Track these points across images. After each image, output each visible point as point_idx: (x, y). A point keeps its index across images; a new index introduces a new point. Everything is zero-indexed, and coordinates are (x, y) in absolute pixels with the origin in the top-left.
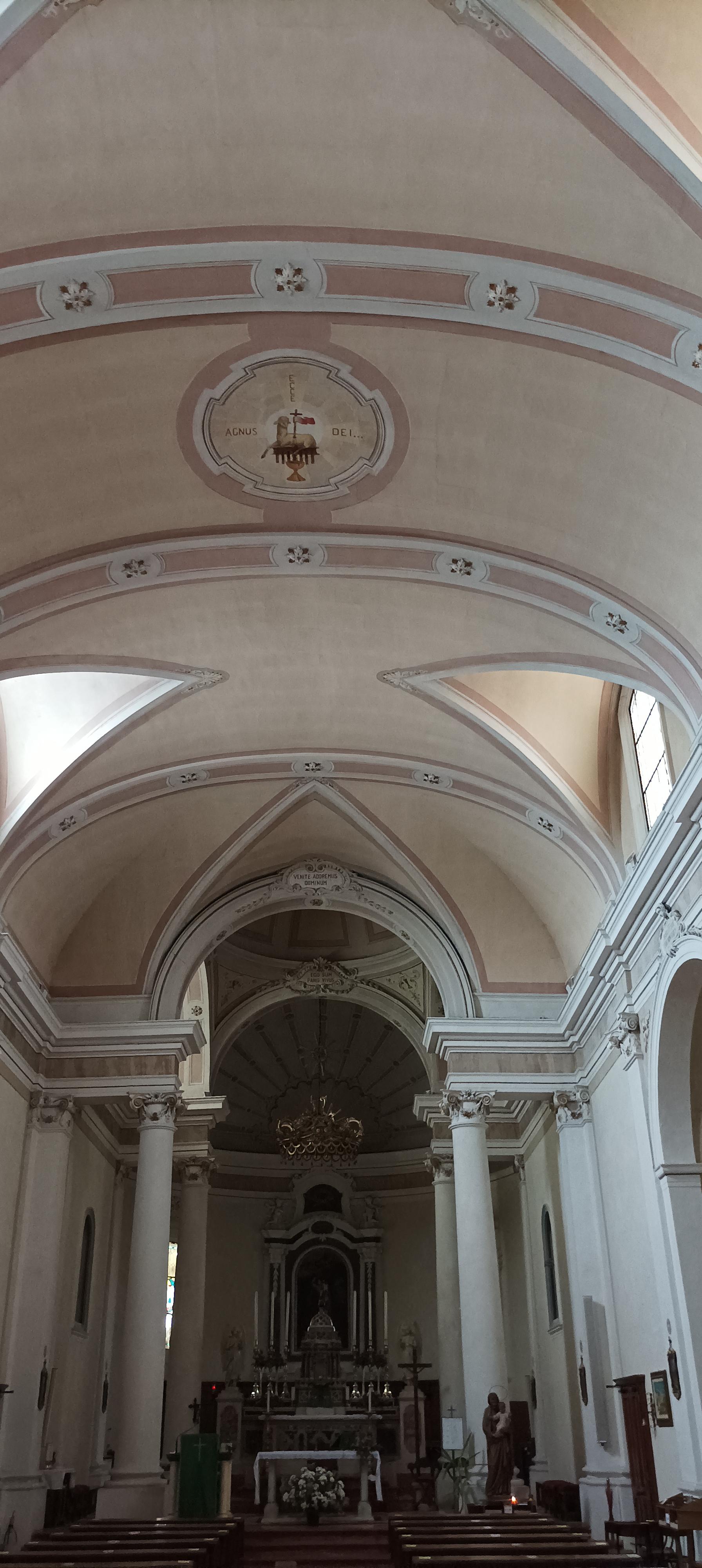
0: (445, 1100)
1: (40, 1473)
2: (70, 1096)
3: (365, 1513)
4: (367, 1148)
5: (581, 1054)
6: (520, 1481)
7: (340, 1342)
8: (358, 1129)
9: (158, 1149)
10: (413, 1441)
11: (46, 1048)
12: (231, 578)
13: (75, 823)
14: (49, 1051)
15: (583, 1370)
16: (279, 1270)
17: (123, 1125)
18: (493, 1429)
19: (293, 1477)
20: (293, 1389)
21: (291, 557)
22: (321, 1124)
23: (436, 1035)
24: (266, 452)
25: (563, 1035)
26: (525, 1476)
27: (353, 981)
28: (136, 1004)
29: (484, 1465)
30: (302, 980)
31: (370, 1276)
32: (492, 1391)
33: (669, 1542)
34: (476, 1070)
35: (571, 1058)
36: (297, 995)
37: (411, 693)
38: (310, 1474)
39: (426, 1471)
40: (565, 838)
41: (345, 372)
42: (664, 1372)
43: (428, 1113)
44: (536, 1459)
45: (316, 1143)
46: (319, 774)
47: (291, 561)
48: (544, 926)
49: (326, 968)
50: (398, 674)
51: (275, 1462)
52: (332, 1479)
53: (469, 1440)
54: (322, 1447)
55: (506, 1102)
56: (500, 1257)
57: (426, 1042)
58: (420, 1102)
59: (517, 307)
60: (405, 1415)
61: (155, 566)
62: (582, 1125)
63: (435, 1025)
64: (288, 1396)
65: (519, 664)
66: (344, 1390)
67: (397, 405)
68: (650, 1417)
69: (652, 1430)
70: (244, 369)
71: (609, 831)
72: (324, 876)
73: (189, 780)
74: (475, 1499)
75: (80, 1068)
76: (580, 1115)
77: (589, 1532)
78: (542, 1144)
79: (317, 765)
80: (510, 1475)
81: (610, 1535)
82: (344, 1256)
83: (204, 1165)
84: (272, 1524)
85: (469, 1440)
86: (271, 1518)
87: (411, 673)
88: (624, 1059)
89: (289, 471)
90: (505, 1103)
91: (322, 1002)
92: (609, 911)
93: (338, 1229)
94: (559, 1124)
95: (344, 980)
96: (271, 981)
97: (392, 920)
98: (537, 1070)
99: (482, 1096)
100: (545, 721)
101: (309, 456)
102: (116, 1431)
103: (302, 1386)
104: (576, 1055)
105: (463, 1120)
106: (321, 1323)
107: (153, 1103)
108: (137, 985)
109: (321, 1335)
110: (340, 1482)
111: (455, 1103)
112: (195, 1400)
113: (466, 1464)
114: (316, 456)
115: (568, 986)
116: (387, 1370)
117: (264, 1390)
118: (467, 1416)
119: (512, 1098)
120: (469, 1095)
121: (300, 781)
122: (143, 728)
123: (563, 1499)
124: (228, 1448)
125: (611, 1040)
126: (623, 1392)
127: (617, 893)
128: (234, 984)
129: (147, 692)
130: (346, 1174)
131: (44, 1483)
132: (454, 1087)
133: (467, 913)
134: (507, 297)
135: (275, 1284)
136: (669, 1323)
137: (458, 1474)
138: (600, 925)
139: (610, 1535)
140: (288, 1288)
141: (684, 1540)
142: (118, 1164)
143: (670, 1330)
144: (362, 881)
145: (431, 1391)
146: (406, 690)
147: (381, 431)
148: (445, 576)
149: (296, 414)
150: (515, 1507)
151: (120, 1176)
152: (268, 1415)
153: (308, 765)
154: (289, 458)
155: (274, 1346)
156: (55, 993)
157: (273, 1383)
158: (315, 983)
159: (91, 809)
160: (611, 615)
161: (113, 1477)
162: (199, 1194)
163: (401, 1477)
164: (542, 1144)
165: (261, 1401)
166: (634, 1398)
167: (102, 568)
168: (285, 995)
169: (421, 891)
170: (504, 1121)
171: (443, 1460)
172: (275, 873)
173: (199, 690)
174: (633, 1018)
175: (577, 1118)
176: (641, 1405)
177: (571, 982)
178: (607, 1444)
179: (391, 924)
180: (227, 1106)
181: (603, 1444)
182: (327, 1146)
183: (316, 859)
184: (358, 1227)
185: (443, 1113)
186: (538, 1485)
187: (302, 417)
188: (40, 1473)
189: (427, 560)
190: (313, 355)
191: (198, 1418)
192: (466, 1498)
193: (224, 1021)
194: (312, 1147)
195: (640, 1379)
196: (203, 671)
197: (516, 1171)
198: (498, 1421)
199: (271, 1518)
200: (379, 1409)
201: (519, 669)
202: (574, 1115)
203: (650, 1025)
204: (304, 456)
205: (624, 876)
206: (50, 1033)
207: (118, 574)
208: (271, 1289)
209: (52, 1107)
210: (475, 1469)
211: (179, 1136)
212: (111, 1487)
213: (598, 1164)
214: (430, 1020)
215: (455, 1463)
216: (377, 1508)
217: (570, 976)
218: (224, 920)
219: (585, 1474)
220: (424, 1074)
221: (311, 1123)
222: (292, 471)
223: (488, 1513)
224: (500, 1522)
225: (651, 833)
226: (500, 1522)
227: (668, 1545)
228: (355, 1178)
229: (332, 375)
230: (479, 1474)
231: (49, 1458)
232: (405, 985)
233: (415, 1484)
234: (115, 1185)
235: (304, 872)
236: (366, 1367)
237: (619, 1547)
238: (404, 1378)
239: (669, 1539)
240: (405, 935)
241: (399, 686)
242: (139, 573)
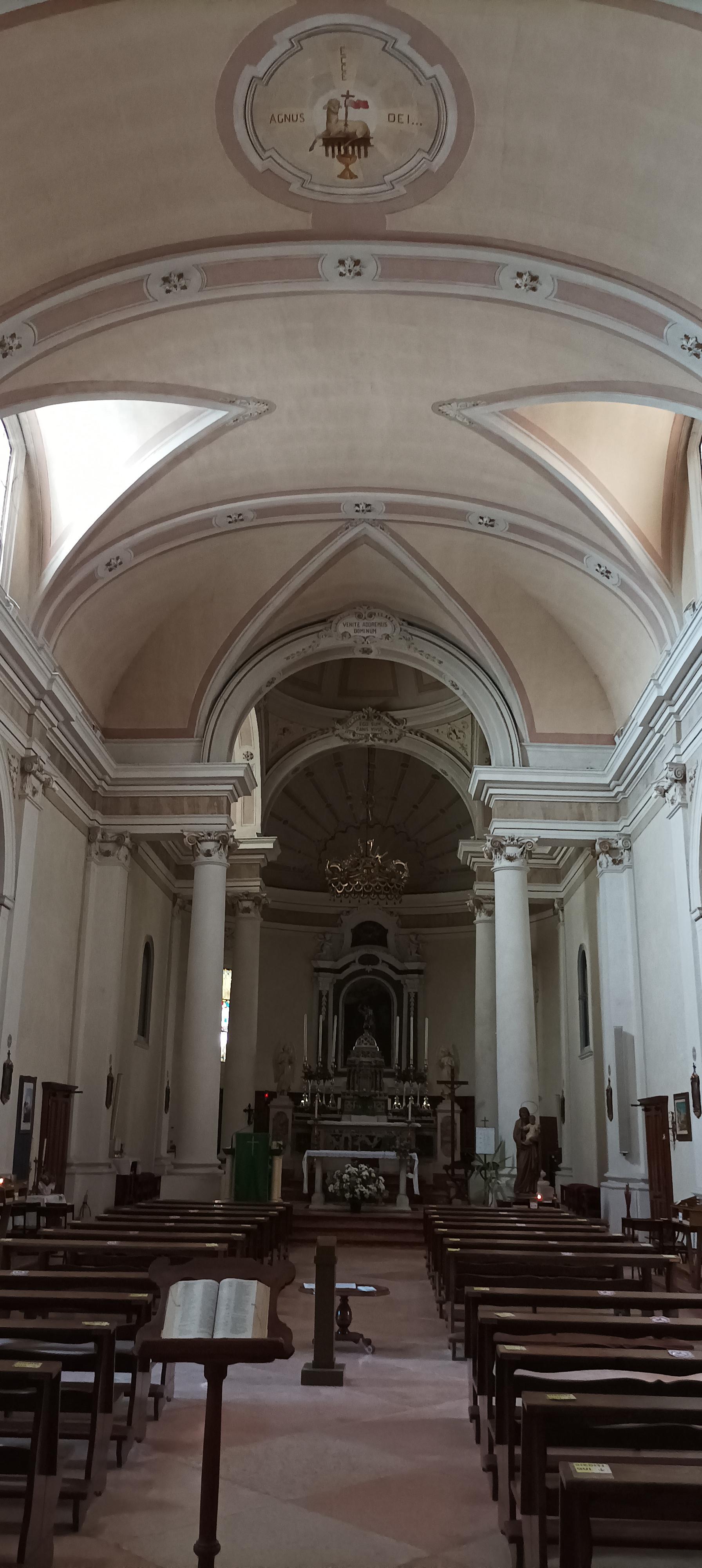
0: (489, 844)
1: (109, 1161)
3: (403, 1204)
4: (413, 888)
5: (626, 803)
6: (547, 1183)
7: (383, 1060)
8: (403, 871)
9: (212, 884)
10: (449, 1146)
11: (102, 787)
14: (104, 789)
15: (610, 1091)
16: (327, 996)
17: (178, 863)
18: (523, 1138)
20: (339, 1099)
23: (482, 783)
24: (315, 142)
25: (609, 785)
26: (551, 1179)
27: (401, 730)
28: (188, 746)
29: (513, 1168)
30: (351, 729)
31: (412, 1004)
32: (524, 1106)
33: (680, 1237)
35: (615, 808)
36: (347, 743)
38: (353, 1170)
39: (460, 1172)
40: (623, 586)
41: (403, 44)
44: (561, 1166)
46: (370, 516)
47: (341, 274)
48: (596, 677)
49: (375, 717)
50: (454, 405)
51: (321, 1159)
53: (500, 1146)
54: (365, 1148)
55: (550, 848)
56: (536, 990)
57: (472, 789)
58: (464, 847)
60: (442, 1124)
61: (195, 280)
62: (623, 870)
63: (481, 773)
64: (335, 1105)
66: (387, 1101)
67: (460, 83)
68: (671, 1132)
69: (671, 1143)
71: (669, 579)
72: (373, 624)
73: (236, 521)
75: (136, 807)
76: (621, 861)
77: (608, 1226)
78: (582, 888)
79: (367, 505)
82: (388, 985)
83: (257, 900)
85: (500, 1146)
86: (317, 1204)
88: (669, 808)
89: (339, 167)
90: (547, 850)
91: (371, 750)
92: (664, 659)
93: (383, 961)
94: (599, 869)
95: (393, 730)
96: (321, 730)
97: (441, 669)
98: (581, 818)
99: (525, 841)
100: (609, 458)
101: (362, 148)
102: (176, 1128)
103: (347, 1097)
104: (621, 806)
105: (505, 863)
106: (366, 1043)
107: (206, 841)
108: (191, 729)
110: (381, 1178)
111: (499, 847)
112: (249, 1106)
114: (369, 149)
116: (426, 1086)
117: (312, 1098)
118: (500, 1124)
119: (555, 844)
120: (513, 840)
121: (350, 522)
122: (187, 464)
123: (586, 1200)
124: (280, 1145)
126: (646, 1110)
127: (673, 643)
128: (284, 731)
129: (190, 423)
130: (392, 913)
131: (114, 1168)
132: (498, 832)
135: (324, 1009)
137: (488, 1175)
138: (653, 675)
140: (336, 1012)
142: (175, 897)
143: (695, 1057)
144: (411, 630)
145: (468, 1105)
147: (443, 118)
149: (348, 96)
150: (540, 1204)
151: (177, 907)
152: (316, 1120)
153: (358, 505)
154: (339, 150)
156: (108, 734)
157: (321, 1095)
159: (138, 549)
161: (177, 1166)
162: (252, 926)
163: (437, 1176)
164: (582, 888)
165: (310, 1109)
166: (656, 1116)
168: (334, 743)
170: (547, 866)
171: (476, 1163)
173: (245, 421)
177: (620, 733)
180: (278, 846)
181: (624, 1154)
183: (365, 607)
184: (402, 961)
186: (563, 1187)
187: (355, 99)
188: (109, 1161)
189: (489, 274)
191: (252, 1120)
192: (496, 1195)
193: (275, 767)
195: (665, 1099)
196: (248, 400)
197: (556, 913)
198: (528, 1131)
199: (317, 1204)
200: (418, 1119)
201: (586, 399)
202: (614, 862)
204: (356, 148)
205: (681, 624)
206: (104, 772)
207: (156, 288)
208: (320, 1013)
209: (111, 842)
210: (505, 1171)
211: (232, 873)
214: (477, 769)
215: (486, 1167)
216: (414, 1200)
217: (619, 727)
218: (274, 666)
219: (606, 1179)
220: (469, 822)
222: (343, 167)
223: (515, 1207)
226: (526, 1215)
227: (680, 1239)
228: (400, 916)
229: (389, 47)
230: (509, 1175)
231: (117, 1148)
232: (453, 736)
233: (449, 1183)
235: (353, 620)
237: (635, 1239)
238: (442, 1093)
239: (681, 1235)
240: (454, 685)
241: (454, 419)
242: (179, 289)
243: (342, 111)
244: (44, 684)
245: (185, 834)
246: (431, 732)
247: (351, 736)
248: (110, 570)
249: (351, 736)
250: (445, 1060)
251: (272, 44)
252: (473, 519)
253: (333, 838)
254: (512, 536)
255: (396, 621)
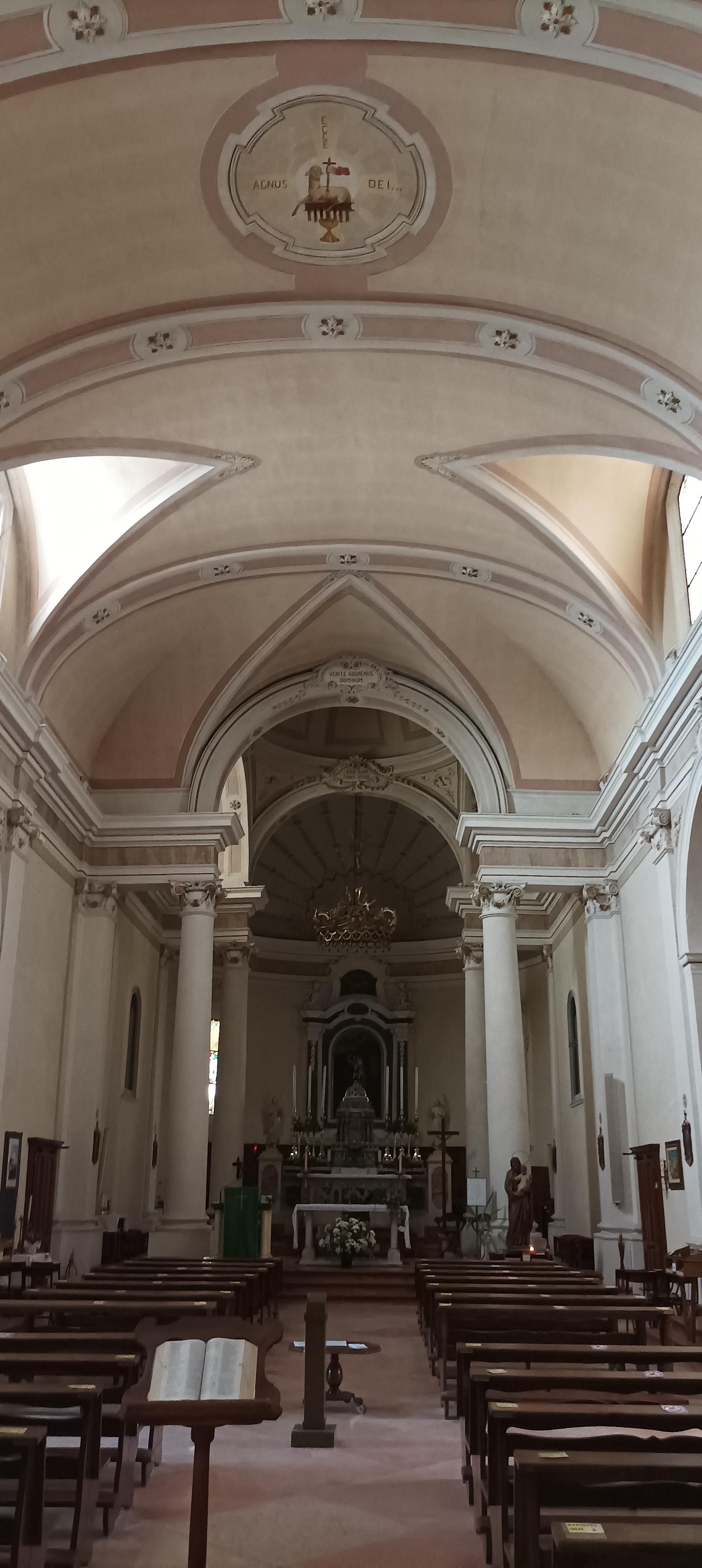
0: (476, 891)
2: (113, 882)
3: (394, 1258)
4: (401, 936)
5: (612, 849)
7: (373, 1111)
9: (199, 934)
12: (262, 353)
13: (108, 615)
15: (601, 1139)
16: (316, 1047)
17: (164, 912)
18: (515, 1189)
19: (328, 1226)
21: (324, 328)
22: (357, 913)
23: (469, 830)
25: (595, 831)
26: (544, 1230)
28: (174, 796)
29: (504, 1219)
30: (338, 776)
31: (402, 1054)
33: (675, 1288)
34: (507, 863)
35: (602, 854)
37: (451, 480)
38: (344, 1224)
39: (451, 1224)
40: (605, 633)
41: (383, 113)
42: (679, 1141)
43: (460, 904)
45: (351, 930)
46: (355, 567)
47: (324, 333)
49: (362, 765)
50: (437, 459)
51: (312, 1213)
52: (364, 1229)
53: (492, 1198)
54: (355, 1201)
56: (526, 1038)
58: (452, 893)
59: (573, 31)
60: (433, 1176)
61: (180, 339)
62: (612, 915)
63: (468, 820)
65: (565, 447)
66: (376, 1153)
68: (663, 1180)
69: (664, 1192)
70: (273, 110)
72: (360, 673)
73: (222, 573)
74: (495, 1248)
75: (122, 857)
76: (608, 907)
79: (353, 557)
80: (530, 1227)
81: (620, 1281)
83: (244, 950)
84: (309, 1266)
85: (492, 1198)
86: (308, 1259)
87: (451, 458)
89: (322, 231)
90: (535, 896)
91: (358, 798)
93: (372, 1011)
94: (587, 915)
95: (380, 778)
98: (568, 864)
100: (588, 511)
102: (164, 1184)
103: (337, 1149)
105: (494, 910)
106: (356, 1094)
108: (178, 778)
109: (355, 1105)
110: (372, 1231)
111: (486, 893)
112: (238, 1159)
113: (488, 1218)
115: (601, 783)
116: (416, 1137)
117: (302, 1150)
119: (543, 890)
121: (335, 574)
123: (578, 1251)
124: (268, 1199)
125: (642, 834)
126: (638, 1158)
127: (655, 690)
132: (485, 879)
133: (502, 712)
134: (563, 19)
135: (313, 1059)
136: (685, 1097)
137: (480, 1227)
138: (636, 722)
139: (620, 1281)
140: (325, 1062)
141: (688, 1287)
142: (162, 948)
143: (685, 1104)
145: (459, 1155)
146: (444, 476)
148: (488, 350)
149: (329, 163)
150: (533, 1256)
151: (164, 959)
152: (305, 1173)
154: (322, 215)
155: (311, 1114)
156: (95, 785)
158: (350, 780)
159: (127, 601)
160: (663, 393)
161: (165, 1222)
162: (239, 977)
163: (428, 1229)
165: (300, 1162)
167: (126, 342)
168: (321, 791)
169: (455, 687)
170: (536, 913)
171: (468, 1215)
172: (311, 670)
173: (229, 476)
174: (665, 813)
175: (606, 910)
176: (654, 1171)
177: (605, 779)
178: (620, 1203)
179: (426, 722)
181: (617, 1204)
182: (362, 934)
183: (351, 656)
185: (474, 904)
187: (336, 166)
188: (96, 1218)
190: (346, 92)
192: (488, 1248)
193: (261, 816)
194: (347, 935)
195: (656, 1147)
197: (545, 960)
198: (519, 1181)
199: (308, 1259)
200: (410, 1170)
201: (565, 452)
203: (682, 821)
204: (338, 213)
206: (91, 823)
207: (142, 348)
208: (309, 1063)
211: (219, 923)
212: (162, 1230)
213: (624, 958)
214: (463, 815)
215: (478, 1219)
216: (406, 1254)
217: (604, 773)
218: (261, 716)
219: (599, 1230)
220: (457, 868)
221: (346, 913)
222: (325, 231)
223: (507, 1260)
224: (519, 1268)
225: (693, 627)
226: (519, 1268)
227: (674, 1291)
229: (369, 117)
230: (501, 1227)
231: (104, 1204)
232: (440, 783)
234: (160, 967)
235: (340, 669)
236: (397, 1134)
237: (629, 1291)
238: (433, 1144)
239: (675, 1286)
240: (440, 733)
241: (437, 472)
242: (165, 348)
243: (323, 179)
244: (31, 736)
245: (172, 884)
246: (418, 779)
247: (338, 784)
248: (98, 622)
249: (338, 784)
250: (437, 1111)
251: (255, 114)
252: (457, 569)
253: (321, 886)
254: (495, 586)
255: (382, 670)
